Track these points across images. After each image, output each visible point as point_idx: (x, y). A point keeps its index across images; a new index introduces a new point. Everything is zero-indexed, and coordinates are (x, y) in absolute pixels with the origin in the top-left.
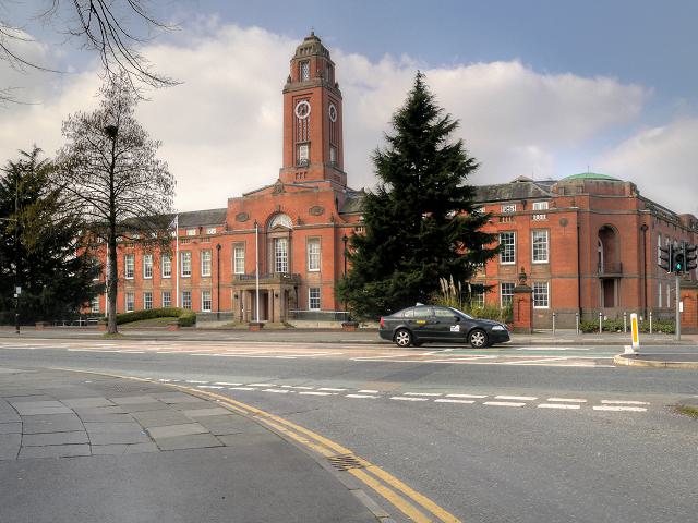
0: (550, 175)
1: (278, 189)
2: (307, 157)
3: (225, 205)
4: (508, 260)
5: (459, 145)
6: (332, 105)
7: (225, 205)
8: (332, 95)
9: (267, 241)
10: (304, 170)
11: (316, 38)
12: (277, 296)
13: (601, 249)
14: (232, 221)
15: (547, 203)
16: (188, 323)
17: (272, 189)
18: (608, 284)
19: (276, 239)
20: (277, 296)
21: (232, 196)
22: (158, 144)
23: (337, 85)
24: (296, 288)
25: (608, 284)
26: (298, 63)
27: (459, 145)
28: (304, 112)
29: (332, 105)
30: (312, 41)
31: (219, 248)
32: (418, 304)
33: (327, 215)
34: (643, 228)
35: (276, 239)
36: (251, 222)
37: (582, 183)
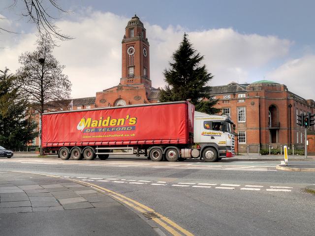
1: (119, 88)
5: (204, 67)
6: (144, 49)
10: (131, 79)
11: (137, 17)
13: (270, 116)
17: (117, 88)
18: (273, 133)
23: (147, 39)
25: (273, 133)
27: (204, 67)
29: (144, 49)
33: (142, 100)
34: (290, 106)
36: (107, 103)
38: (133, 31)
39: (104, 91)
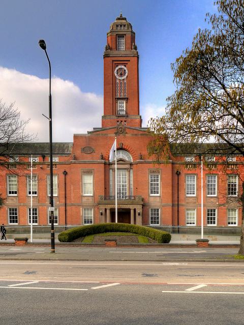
28: (121, 75)
31: (65, 173)
38: (123, 41)
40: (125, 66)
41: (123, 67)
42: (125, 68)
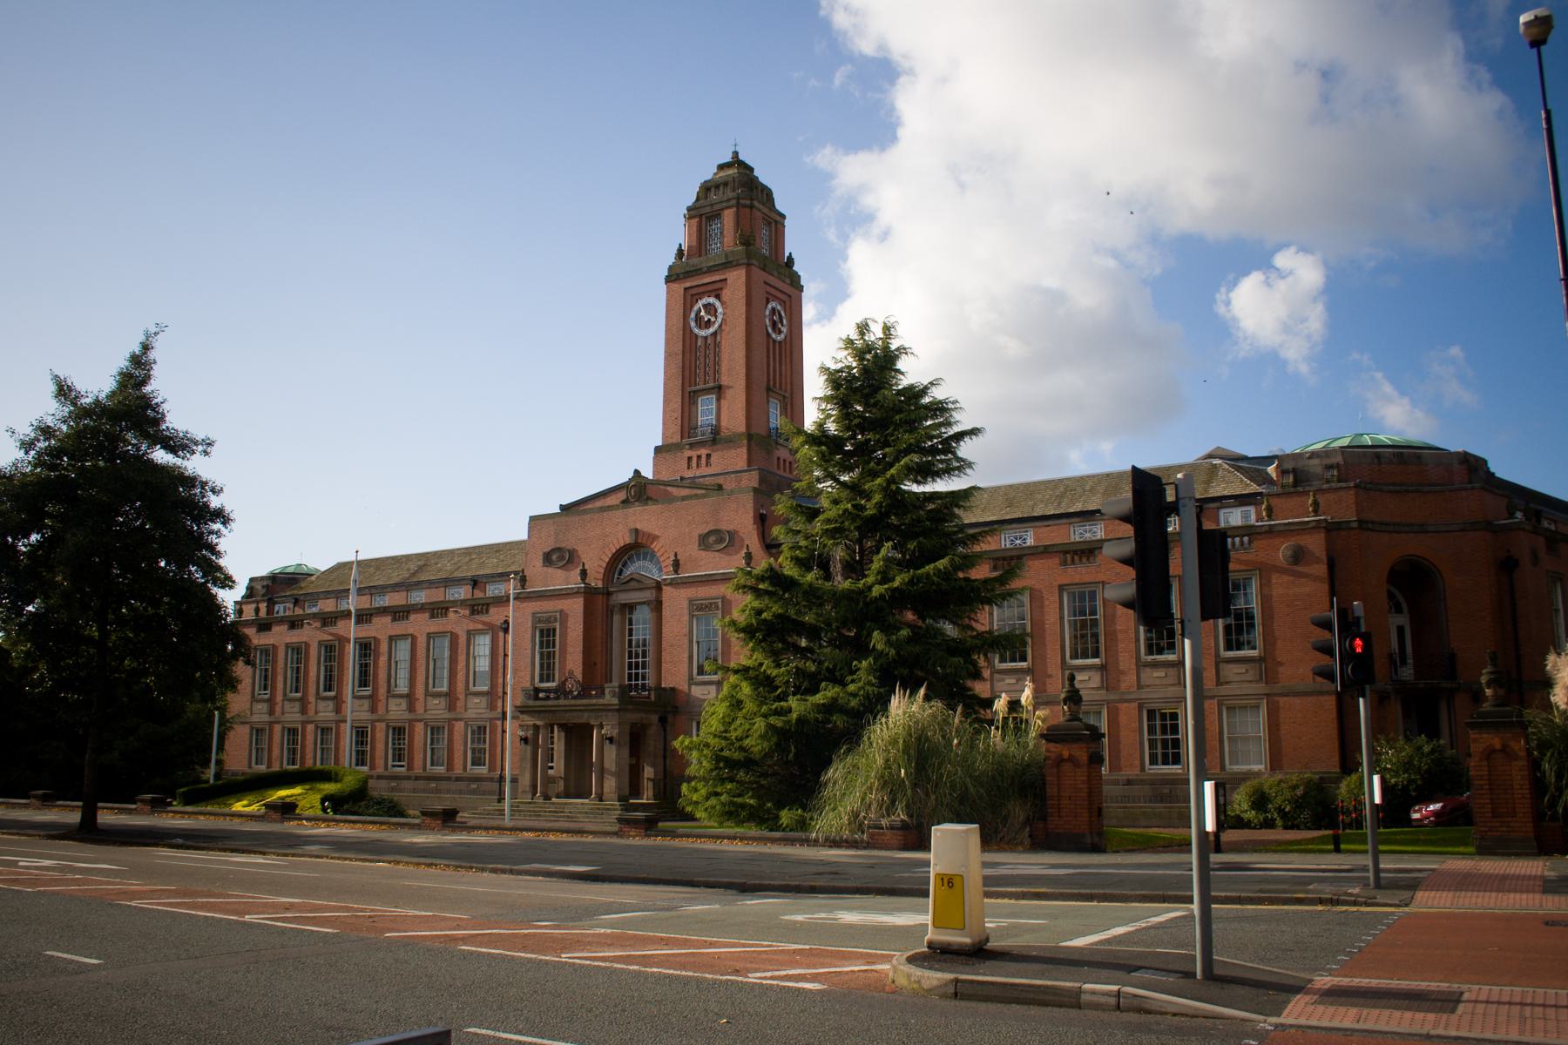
0: (115, 371)
1: (637, 490)
2: (712, 418)
3: (520, 533)
4: (1160, 652)
7: (520, 533)
8: (773, 280)
9: (609, 612)
10: (703, 452)
12: (611, 740)
14: (535, 568)
15: (1252, 509)
16: (392, 810)
19: (631, 607)
20: (611, 740)
21: (1140, 466)
22: (64, 391)
24: (663, 720)
26: (702, 214)
30: (732, 171)
32: (1455, 351)
34: (1508, 566)
35: (631, 607)
37: (1339, 459)
39: (564, 508)
40: (718, 297)
41: (712, 300)
42: (718, 304)
